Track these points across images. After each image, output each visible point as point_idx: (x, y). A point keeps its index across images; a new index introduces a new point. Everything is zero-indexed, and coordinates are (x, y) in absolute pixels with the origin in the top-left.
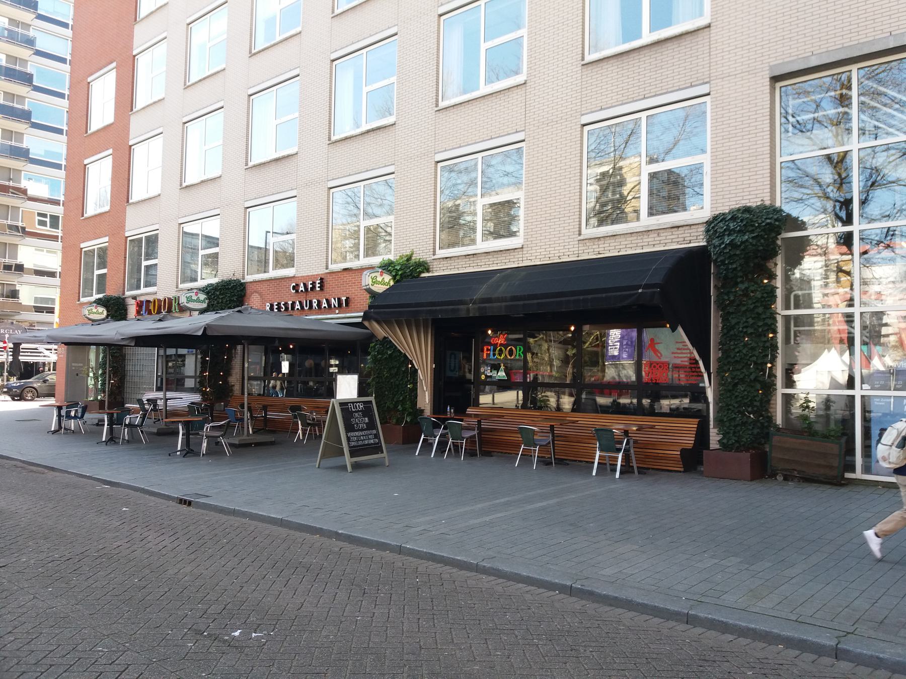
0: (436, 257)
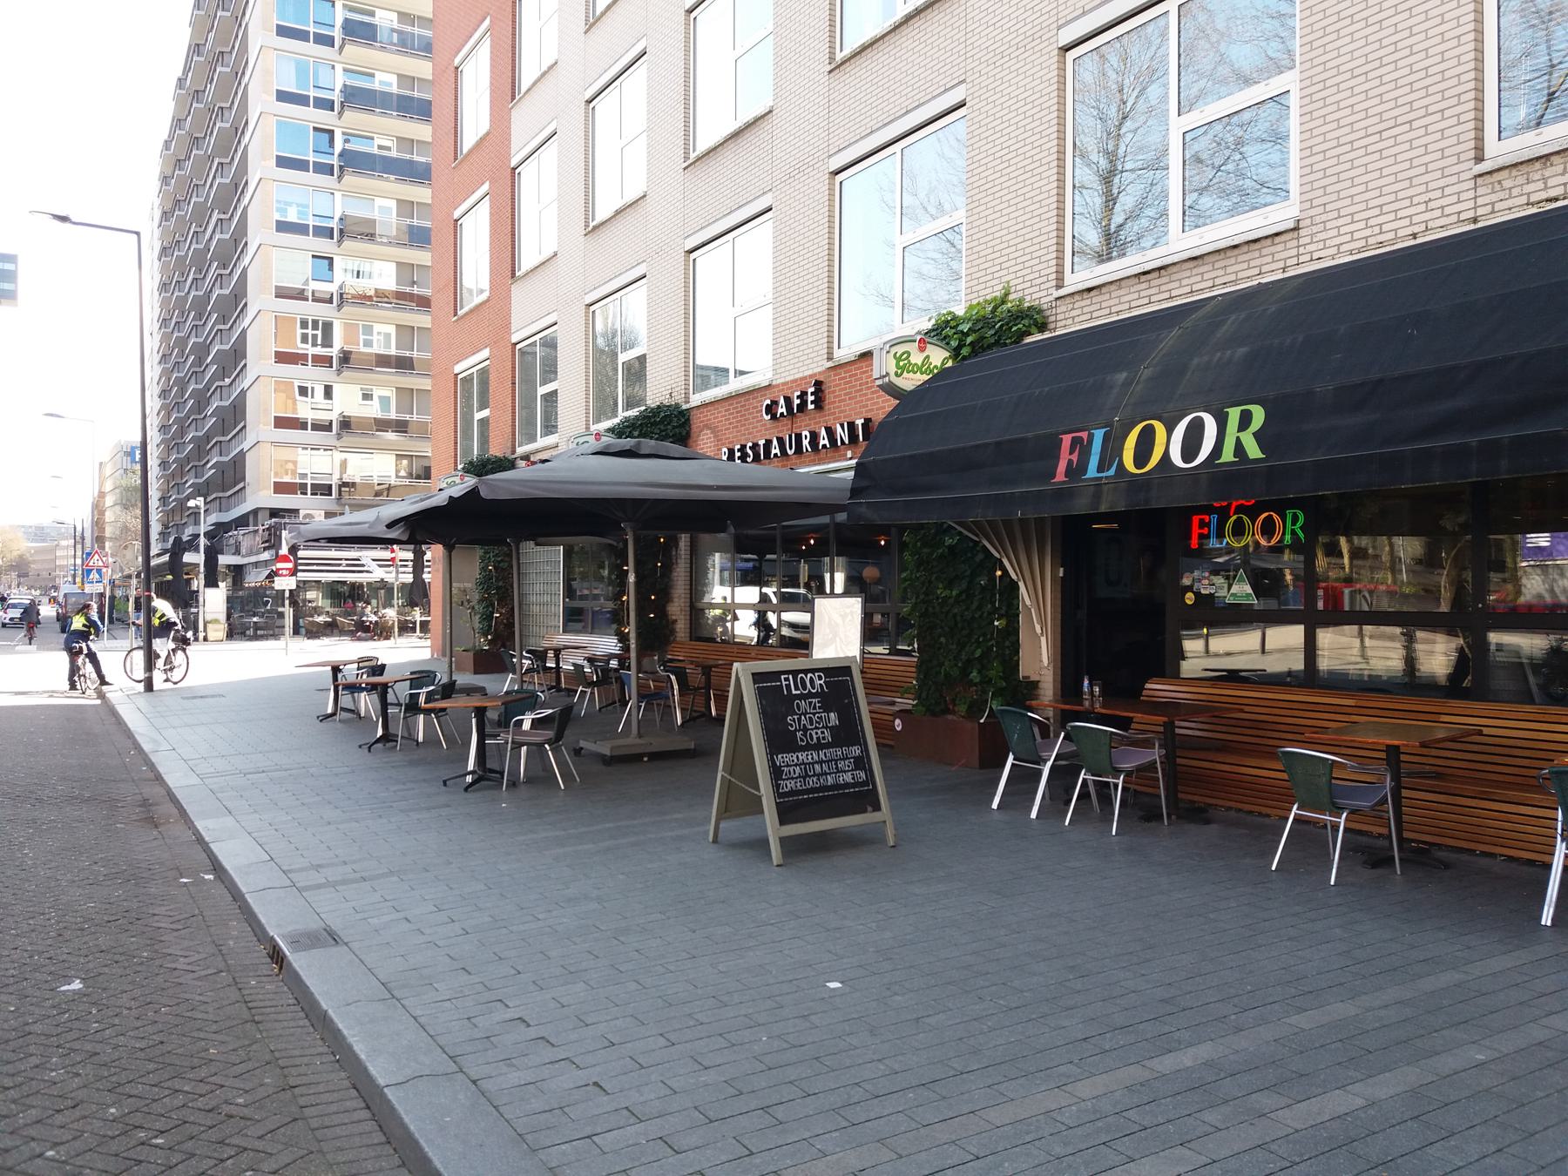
0: (1062, 292)
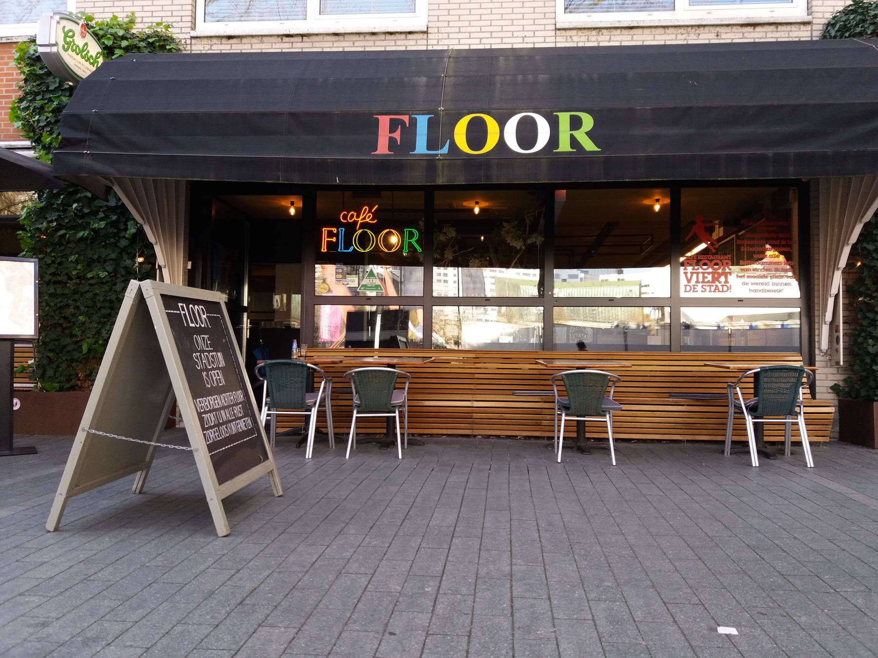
0: (193, 34)
